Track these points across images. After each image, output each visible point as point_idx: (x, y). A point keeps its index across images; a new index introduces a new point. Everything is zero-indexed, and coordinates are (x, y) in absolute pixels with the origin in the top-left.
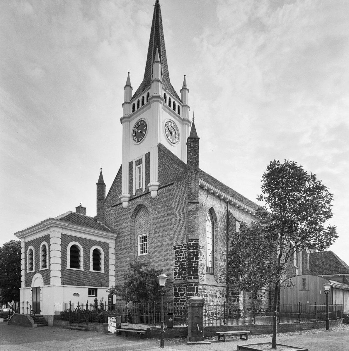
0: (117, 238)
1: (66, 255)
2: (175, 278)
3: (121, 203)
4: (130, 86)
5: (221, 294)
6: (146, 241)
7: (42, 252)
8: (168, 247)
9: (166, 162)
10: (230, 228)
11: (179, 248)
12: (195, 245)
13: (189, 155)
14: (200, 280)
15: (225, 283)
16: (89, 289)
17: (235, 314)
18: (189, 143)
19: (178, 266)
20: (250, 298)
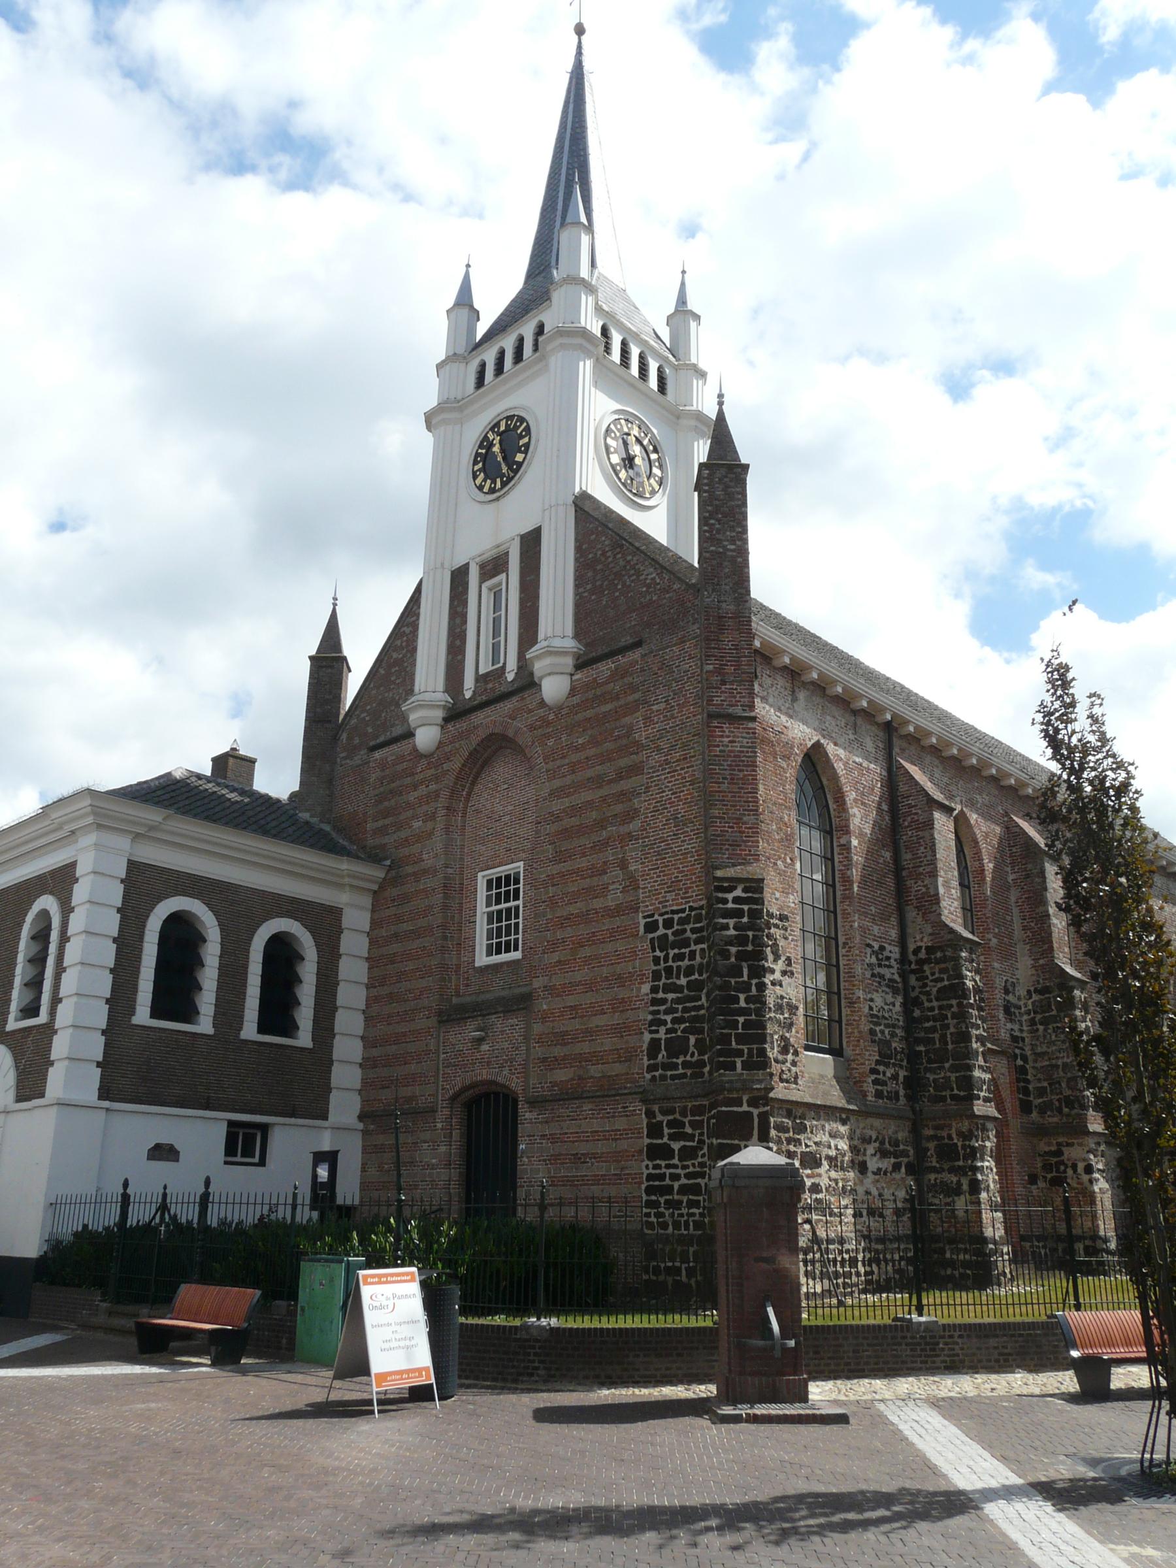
0: (383, 885)
1: (139, 958)
2: (652, 1068)
3: (410, 734)
4: (471, 307)
5: (883, 1153)
6: (516, 898)
7: (32, 942)
8: (617, 922)
9: (610, 559)
10: (908, 835)
11: (668, 924)
12: (746, 907)
13: (706, 528)
14: (776, 1078)
15: (902, 1100)
16: (231, 1124)
17: (966, 1264)
18: (706, 485)
19: (666, 1012)
20: (1033, 1179)
